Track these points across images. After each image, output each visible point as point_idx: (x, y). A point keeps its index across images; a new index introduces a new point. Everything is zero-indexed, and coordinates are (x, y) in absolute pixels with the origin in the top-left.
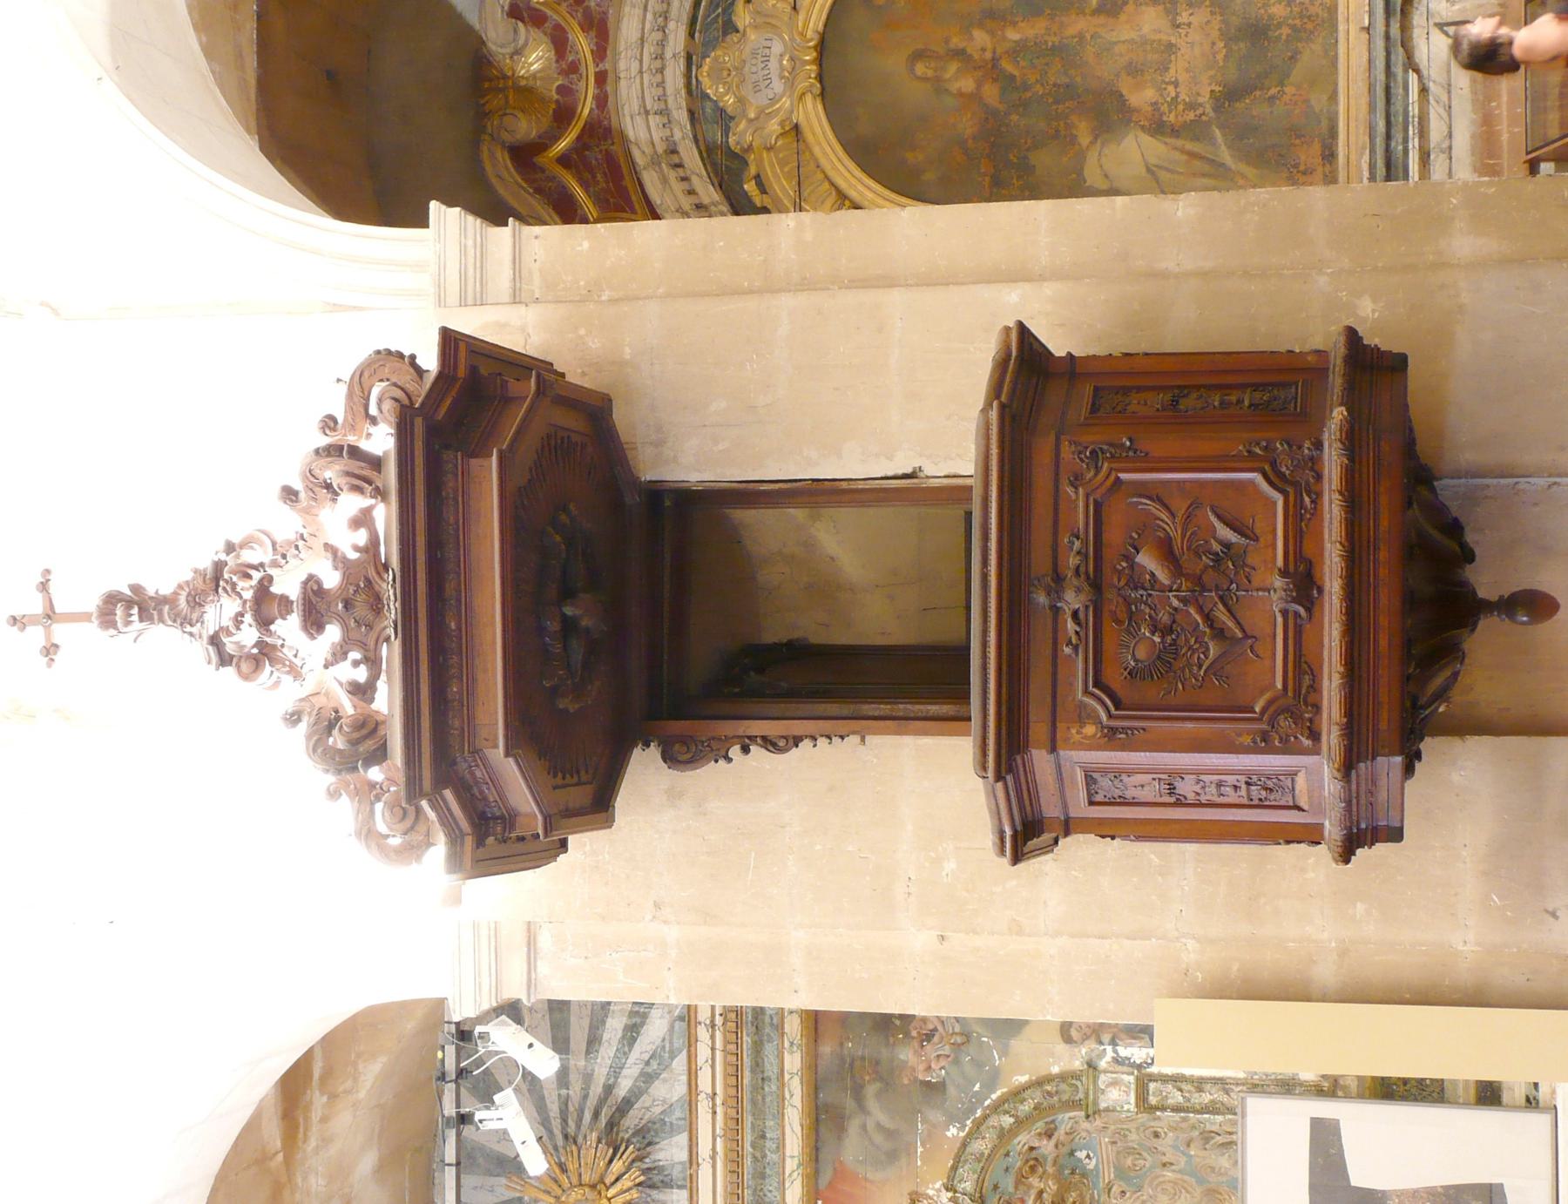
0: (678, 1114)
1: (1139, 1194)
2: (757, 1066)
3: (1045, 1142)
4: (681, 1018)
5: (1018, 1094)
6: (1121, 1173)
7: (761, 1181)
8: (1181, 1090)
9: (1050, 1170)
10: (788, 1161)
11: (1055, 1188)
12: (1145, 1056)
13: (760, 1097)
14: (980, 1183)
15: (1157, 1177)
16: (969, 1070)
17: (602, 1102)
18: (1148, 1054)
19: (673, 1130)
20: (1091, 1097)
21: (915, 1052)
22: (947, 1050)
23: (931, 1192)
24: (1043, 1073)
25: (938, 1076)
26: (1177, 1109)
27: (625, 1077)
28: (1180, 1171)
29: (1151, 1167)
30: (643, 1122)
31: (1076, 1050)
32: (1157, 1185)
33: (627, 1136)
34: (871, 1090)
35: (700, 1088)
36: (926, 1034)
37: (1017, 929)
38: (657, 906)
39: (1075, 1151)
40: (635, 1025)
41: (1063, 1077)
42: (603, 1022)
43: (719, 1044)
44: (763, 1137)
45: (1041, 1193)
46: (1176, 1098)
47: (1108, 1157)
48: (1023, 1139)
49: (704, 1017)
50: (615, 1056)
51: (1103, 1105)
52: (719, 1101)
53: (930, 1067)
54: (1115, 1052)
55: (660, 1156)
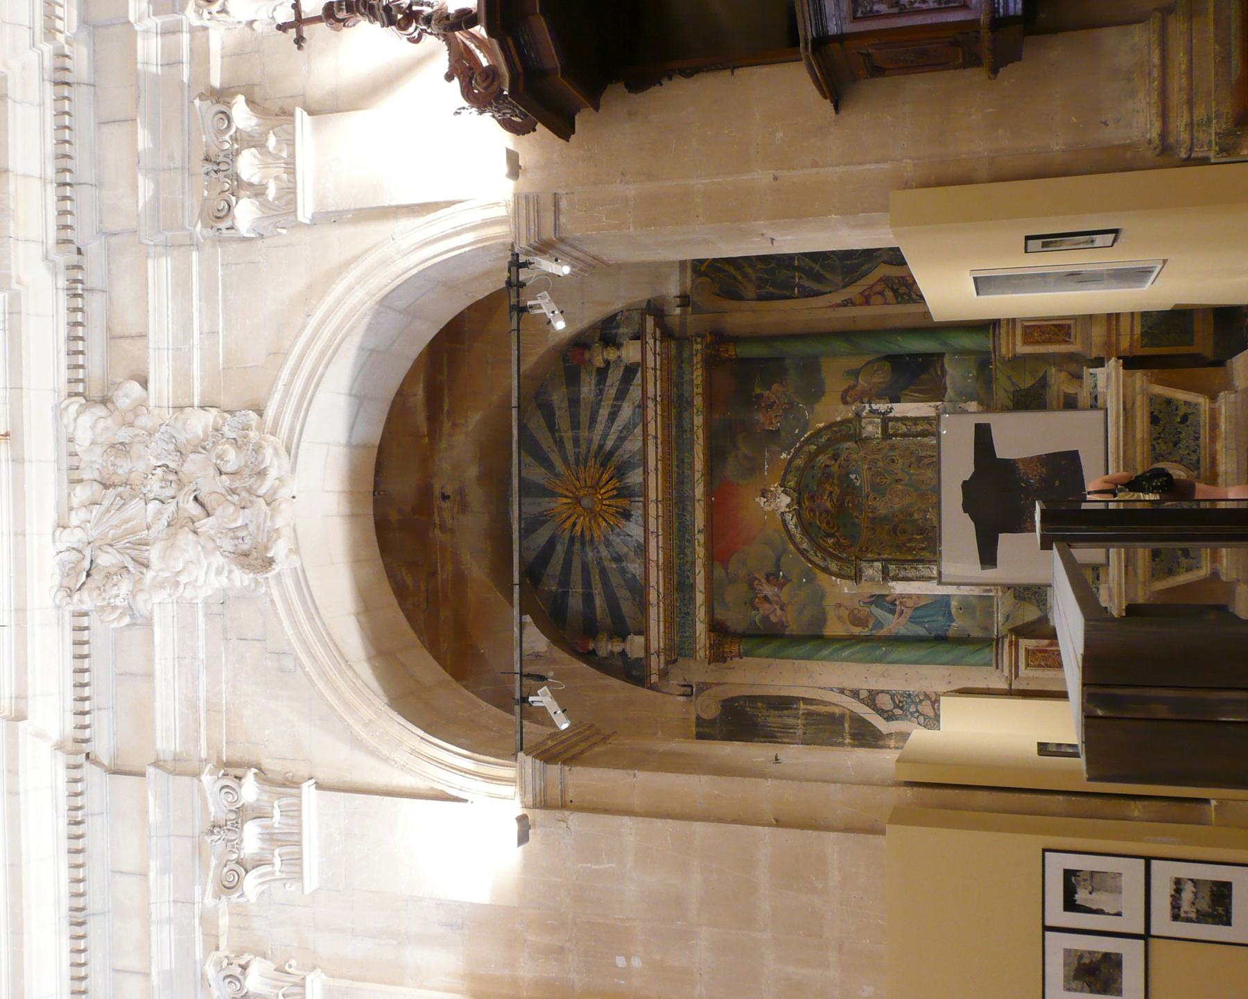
0: (638, 457)
3: (833, 462)
4: (639, 406)
5: (819, 433)
8: (905, 425)
9: (836, 482)
10: (696, 474)
11: (839, 491)
14: (798, 483)
19: (635, 466)
23: (772, 489)
24: (832, 420)
28: (905, 485)
37: (815, 164)
38: (623, 174)
40: (615, 411)
42: (598, 412)
43: (659, 412)
45: (831, 493)
46: (904, 429)
48: (822, 459)
51: (864, 435)
52: (659, 442)
55: (628, 480)
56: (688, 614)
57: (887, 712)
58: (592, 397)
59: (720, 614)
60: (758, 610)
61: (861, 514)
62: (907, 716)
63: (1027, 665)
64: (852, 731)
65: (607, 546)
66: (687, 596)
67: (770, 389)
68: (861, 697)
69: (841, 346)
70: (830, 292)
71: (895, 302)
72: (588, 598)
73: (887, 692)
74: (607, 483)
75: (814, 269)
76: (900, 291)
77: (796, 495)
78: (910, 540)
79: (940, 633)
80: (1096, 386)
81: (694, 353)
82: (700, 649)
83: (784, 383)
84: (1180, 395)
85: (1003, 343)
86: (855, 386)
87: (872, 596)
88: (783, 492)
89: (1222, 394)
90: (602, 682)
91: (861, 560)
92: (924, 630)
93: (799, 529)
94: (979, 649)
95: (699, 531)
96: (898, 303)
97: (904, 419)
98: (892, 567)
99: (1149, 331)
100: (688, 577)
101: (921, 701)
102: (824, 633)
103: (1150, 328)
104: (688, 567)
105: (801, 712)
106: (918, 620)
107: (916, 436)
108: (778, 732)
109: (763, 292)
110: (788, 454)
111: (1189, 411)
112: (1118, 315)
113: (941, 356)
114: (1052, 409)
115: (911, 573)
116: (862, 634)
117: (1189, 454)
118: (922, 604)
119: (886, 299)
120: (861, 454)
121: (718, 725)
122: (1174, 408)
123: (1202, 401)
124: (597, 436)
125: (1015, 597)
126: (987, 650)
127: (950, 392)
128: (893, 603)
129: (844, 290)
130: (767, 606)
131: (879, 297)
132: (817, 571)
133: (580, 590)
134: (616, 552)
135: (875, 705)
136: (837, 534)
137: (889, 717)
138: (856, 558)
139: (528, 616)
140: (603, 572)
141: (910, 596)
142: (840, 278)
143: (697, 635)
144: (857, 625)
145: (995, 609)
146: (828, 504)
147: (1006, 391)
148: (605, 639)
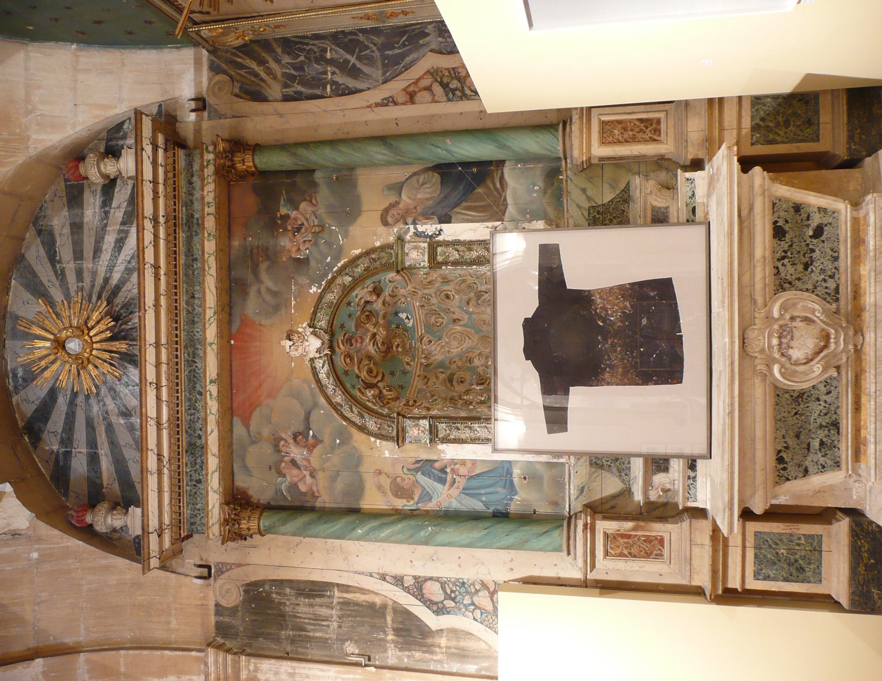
1: (440, 342)
2: (189, 252)
3: (374, 298)
5: (354, 261)
6: (429, 328)
7: (191, 326)
8: (458, 251)
9: (381, 321)
10: (208, 311)
12: (434, 230)
13: (191, 272)
14: (331, 323)
15: (451, 330)
16: (324, 249)
17: (103, 288)
18: (436, 228)
20: (400, 259)
21: (290, 239)
22: (310, 237)
23: (300, 330)
24: (370, 246)
25: (305, 254)
26: (455, 263)
27: (116, 272)
28: (464, 325)
29: (447, 324)
30: (127, 299)
31: (391, 230)
32: (451, 335)
33: (118, 309)
34: (263, 266)
35: (146, 260)
36: (297, 228)
39: (399, 312)
41: (383, 248)
42: (103, 238)
44: (193, 297)
45: (374, 336)
47: (420, 319)
48: (362, 293)
49: (149, 213)
50: (110, 259)
51: (407, 264)
53: (299, 249)
54: (415, 228)
56: (199, 481)
57: (436, 603)
58: (96, 221)
59: (241, 481)
60: (284, 476)
61: (412, 360)
62: (460, 609)
63: (606, 554)
64: (395, 626)
65: (114, 398)
66: (199, 461)
67: (297, 209)
68: (406, 585)
69: (378, 152)
70: (369, 89)
71: (445, 99)
72: (93, 459)
73: (437, 580)
74: (98, 322)
75: (349, 62)
76: (452, 86)
77: (327, 337)
78: (467, 392)
79: (499, 508)
80: (693, 195)
81: (205, 163)
82: (213, 524)
83: (314, 202)
84: (813, 199)
85: (576, 142)
86: (397, 203)
87: (418, 462)
88: (312, 333)
89: (869, 197)
90: (104, 562)
91: (404, 417)
92: (481, 504)
93: (331, 378)
94: (546, 532)
95: (211, 382)
96: (449, 100)
97: (455, 243)
98: (442, 426)
99: (761, 123)
100: (200, 437)
101: (477, 591)
102: (362, 506)
103: (763, 119)
104: (198, 425)
105: (335, 601)
106: (471, 492)
107: (473, 262)
108: (309, 624)
109: (290, 91)
110: (318, 288)
111: (825, 221)
112: (721, 100)
113: (501, 163)
114: (636, 225)
115: (466, 434)
116: (406, 508)
117: (825, 280)
118: (478, 471)
119: (434, 95)
120: (409, 287)
121: (240, 614)
122: (804, 216)
123: (842, 207)
124: (102, 270)
125: (591, 464)
126: (556, 533)
127: (511, 210)
128: (443, 470)
129: (385, 86)
130: (295, 472)
131: (426, 95)
132: (353, 430)
133: (84, 450)
134: (125, 406)
135: (423, 597)
136: (380, 385)
137: (439, 610)
138: (399, 414)
139: (8, 484)
140: (110, 428)
141: (463, 462)
142: (380, 72)
143: (210, 507)
144: (401, 497)
145: (567, 479)
146: (371, 349)
147: (579, 207)
148: (103, 511)
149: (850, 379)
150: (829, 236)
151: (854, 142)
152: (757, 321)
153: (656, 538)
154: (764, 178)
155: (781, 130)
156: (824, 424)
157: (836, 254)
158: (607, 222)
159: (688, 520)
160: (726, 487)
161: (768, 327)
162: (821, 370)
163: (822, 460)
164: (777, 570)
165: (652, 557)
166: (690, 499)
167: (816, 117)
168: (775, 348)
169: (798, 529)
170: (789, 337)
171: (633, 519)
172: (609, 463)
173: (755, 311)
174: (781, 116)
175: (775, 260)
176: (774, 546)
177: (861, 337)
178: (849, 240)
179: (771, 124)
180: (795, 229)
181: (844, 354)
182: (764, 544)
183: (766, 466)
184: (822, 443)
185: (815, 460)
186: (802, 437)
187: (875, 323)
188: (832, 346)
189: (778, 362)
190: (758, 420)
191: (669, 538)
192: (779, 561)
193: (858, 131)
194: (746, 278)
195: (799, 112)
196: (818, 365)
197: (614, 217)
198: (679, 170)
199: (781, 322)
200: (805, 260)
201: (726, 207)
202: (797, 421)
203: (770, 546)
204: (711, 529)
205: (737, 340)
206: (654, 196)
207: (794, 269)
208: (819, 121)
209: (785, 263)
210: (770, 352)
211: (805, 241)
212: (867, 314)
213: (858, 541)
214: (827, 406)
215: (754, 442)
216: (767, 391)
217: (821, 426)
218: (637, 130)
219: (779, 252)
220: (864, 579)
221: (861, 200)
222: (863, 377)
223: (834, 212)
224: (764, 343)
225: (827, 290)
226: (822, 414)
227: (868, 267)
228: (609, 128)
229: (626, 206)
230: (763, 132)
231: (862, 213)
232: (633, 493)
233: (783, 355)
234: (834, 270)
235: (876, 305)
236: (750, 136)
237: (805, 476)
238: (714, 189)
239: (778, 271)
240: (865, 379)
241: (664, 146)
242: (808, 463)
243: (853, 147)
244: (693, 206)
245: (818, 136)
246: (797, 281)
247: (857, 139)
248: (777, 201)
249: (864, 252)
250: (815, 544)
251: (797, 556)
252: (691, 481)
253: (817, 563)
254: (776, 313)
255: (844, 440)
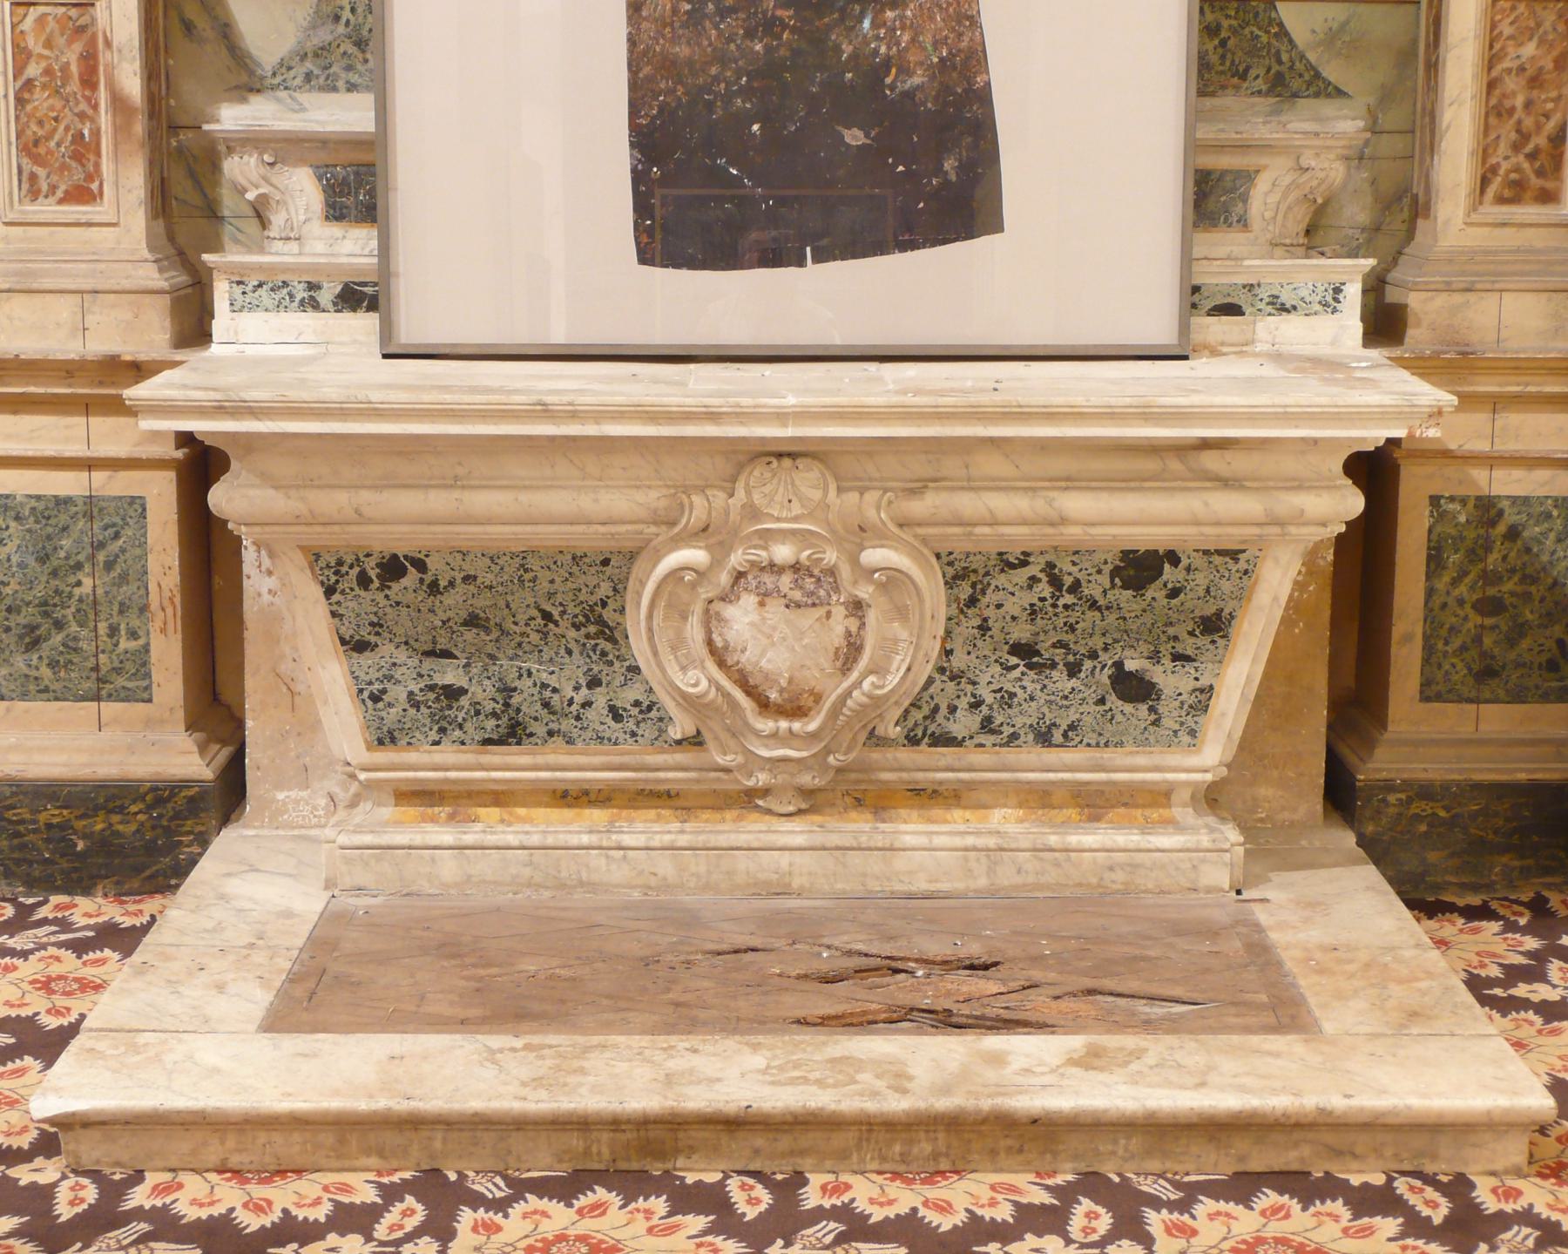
80: (1283, 309)
99: (1501, 528)
103: (1513, 533)
114: (1193, 118)
117: (976, 705)
122: (1188, 646)
149: (662, 775)
150: (1119, 717)
151: (1410, 800)
152: (853, 497)
153: (94, 174)
154: (1324, 525)
155: (1472, 588)
156: (516, 700)
157: (1057, 737)
158: (1209, 17)
159: (164, 285)
160: (293, 395)
161: (833, 532)
162: (691, 690)
163: (398, 693)
164: (22, 565)
165: (25, 161)
166: (238, 290)
167: (1502, 693)
168: (764, 554)
169: (163, 631)
170: (797, 595)
171: (152, 98)
172: (346, 14)
173: (886, 491)
174: (1519, 589)
175: (1050, 557)
176: (101, 557)
177: (791, 809)
178: (1102, 776)
179: (1493, 559)
180: (1148, 619)
181: (740, 759)
182: (106, 528)
183: (371, 521)
184: (452, 693)
185: (398, 673)
186: (470, 635)
187: (838, 848)
188: (766, 725)
189: (717, 562)
190: (525, 497)
191: (97, 219)
192: (54, 573)
193: (1442, 814)
194: (993, 465)
195: (1525, 644)
196: (704, 684)
197: (1223, 43)
198: (1371, 262)
199: (845, 572)
200: (1045, 647)
201: (1229, 400)
202: (521, 618)
203: (102, 545)
204: (142, 357)
205: (790, 432)
206: (1287, 180)
207: (1016, 611)
208: (1487, 701)
209: (1038, 588)
210: (749, 537)
211: (1106, 649)
212: (867, 827)
213: (141, 806)
214: (574, 707)
215: (446, 487)
216: (623, 528)
217: (508, 691)
218: (1529, 123)
219: (1074, 569)
220: (22, 822)
221: (1225, 814)
222: (666, 812)
223: (1193, 733)
224: (778, 520)
225: (944, 710)
226: (547, 694)
227: (1012, 828)
228: (1547, 25)
229: (1260, 84)
230: (1471, 534)
231: (1182, 812)
232: (244, 100)
233: (740, 575)
234: (1007, 730)
235: (892, 849)
236: (1461, 491)
237: (343, 642)
238: (1295, 370)
239: (1012, 566)
240: (659, 819)
241: (1461, 212)
242: (387, 651)
243: (1392, 798)
244: (1248, 310)
245: (1438, 697)
246: (977, 622)
247: (1415, 809)
248: (1242, 565)
249: (1060, 819)
250: (121, 681)
251: (74, 628)
252: (301, 294)
253: (56, 686)
254: (874, 556)
255: (468, 757)
